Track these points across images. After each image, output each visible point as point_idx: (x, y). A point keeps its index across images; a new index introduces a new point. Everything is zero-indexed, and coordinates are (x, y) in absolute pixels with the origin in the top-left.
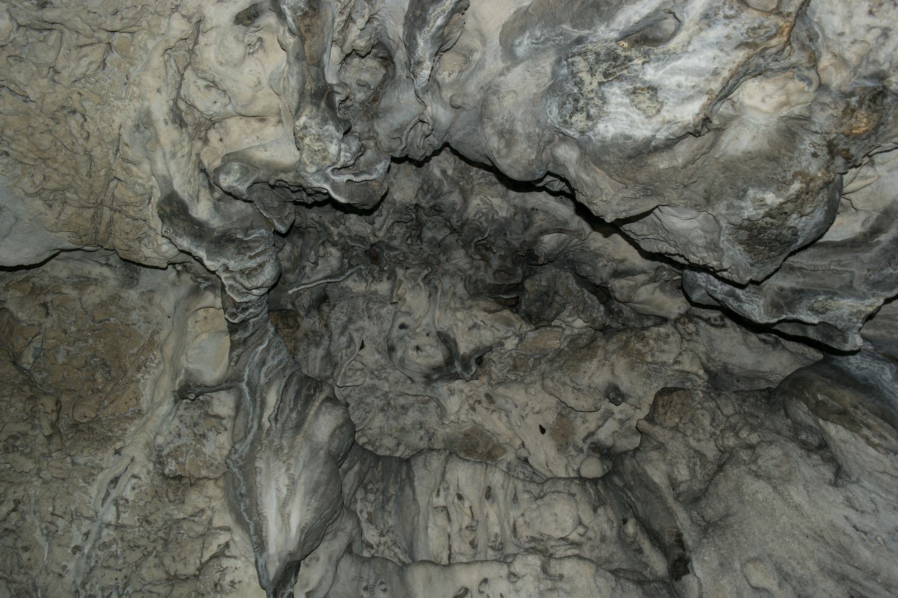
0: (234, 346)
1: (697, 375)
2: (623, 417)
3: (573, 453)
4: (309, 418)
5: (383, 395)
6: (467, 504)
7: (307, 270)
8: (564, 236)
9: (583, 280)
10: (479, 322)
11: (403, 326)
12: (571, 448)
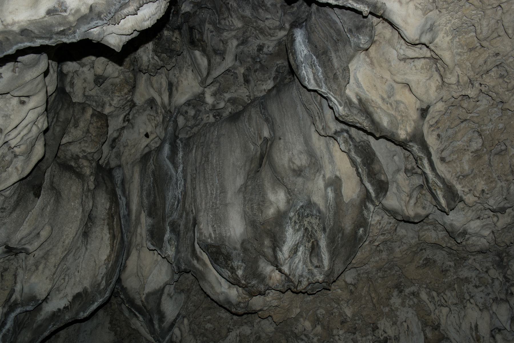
2: (80, 72)
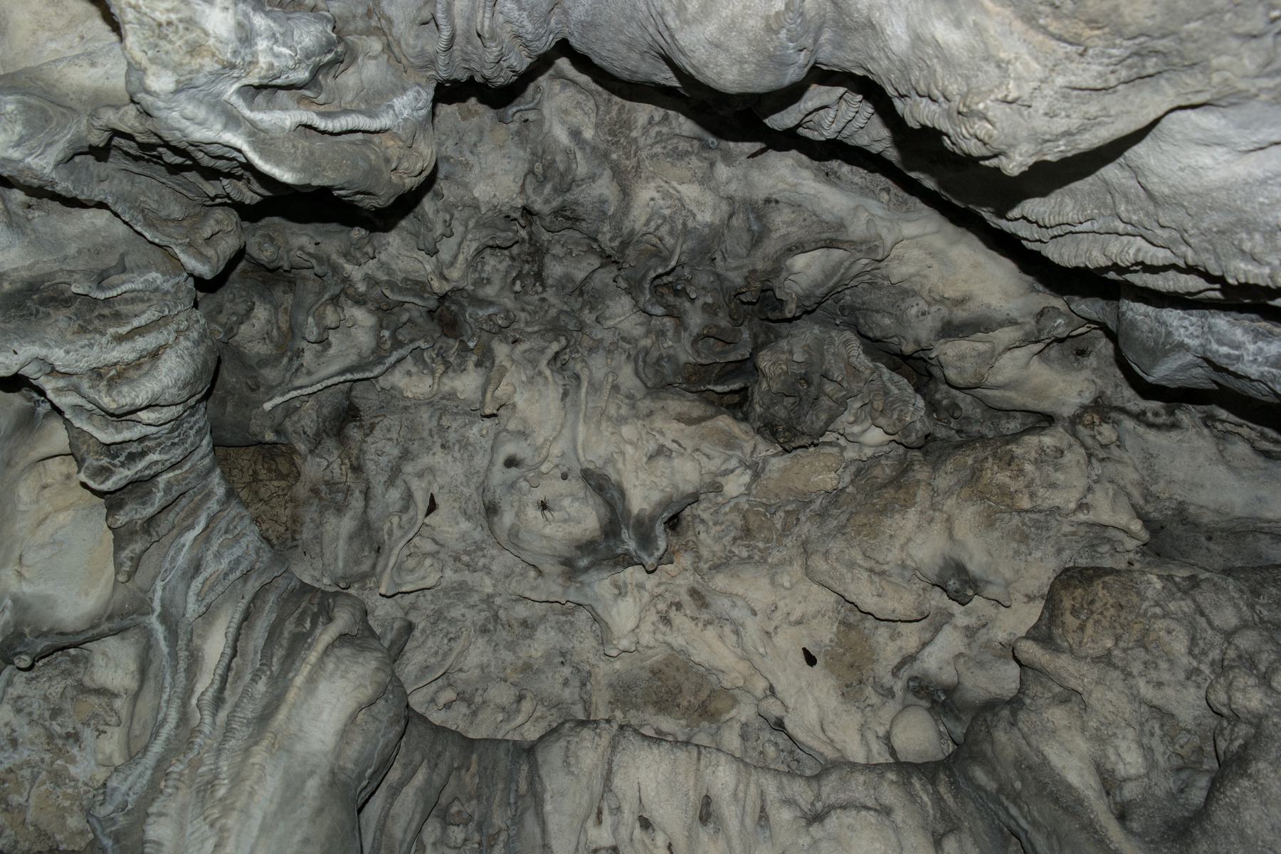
0: (121, 538)
1: (1126, 532)
3: (875, 699)
4: (291, 695)
5: (482, 601)
6: (661, 840)
7: (308, 357)
8: (837, 254)
9: (877, 347)
10: (668, 444)
11: (511, 462)
12: (869, 691)
